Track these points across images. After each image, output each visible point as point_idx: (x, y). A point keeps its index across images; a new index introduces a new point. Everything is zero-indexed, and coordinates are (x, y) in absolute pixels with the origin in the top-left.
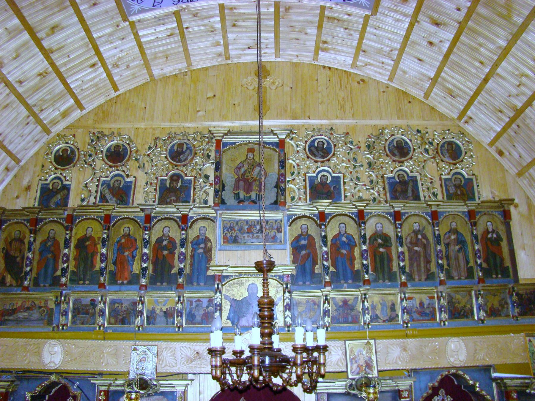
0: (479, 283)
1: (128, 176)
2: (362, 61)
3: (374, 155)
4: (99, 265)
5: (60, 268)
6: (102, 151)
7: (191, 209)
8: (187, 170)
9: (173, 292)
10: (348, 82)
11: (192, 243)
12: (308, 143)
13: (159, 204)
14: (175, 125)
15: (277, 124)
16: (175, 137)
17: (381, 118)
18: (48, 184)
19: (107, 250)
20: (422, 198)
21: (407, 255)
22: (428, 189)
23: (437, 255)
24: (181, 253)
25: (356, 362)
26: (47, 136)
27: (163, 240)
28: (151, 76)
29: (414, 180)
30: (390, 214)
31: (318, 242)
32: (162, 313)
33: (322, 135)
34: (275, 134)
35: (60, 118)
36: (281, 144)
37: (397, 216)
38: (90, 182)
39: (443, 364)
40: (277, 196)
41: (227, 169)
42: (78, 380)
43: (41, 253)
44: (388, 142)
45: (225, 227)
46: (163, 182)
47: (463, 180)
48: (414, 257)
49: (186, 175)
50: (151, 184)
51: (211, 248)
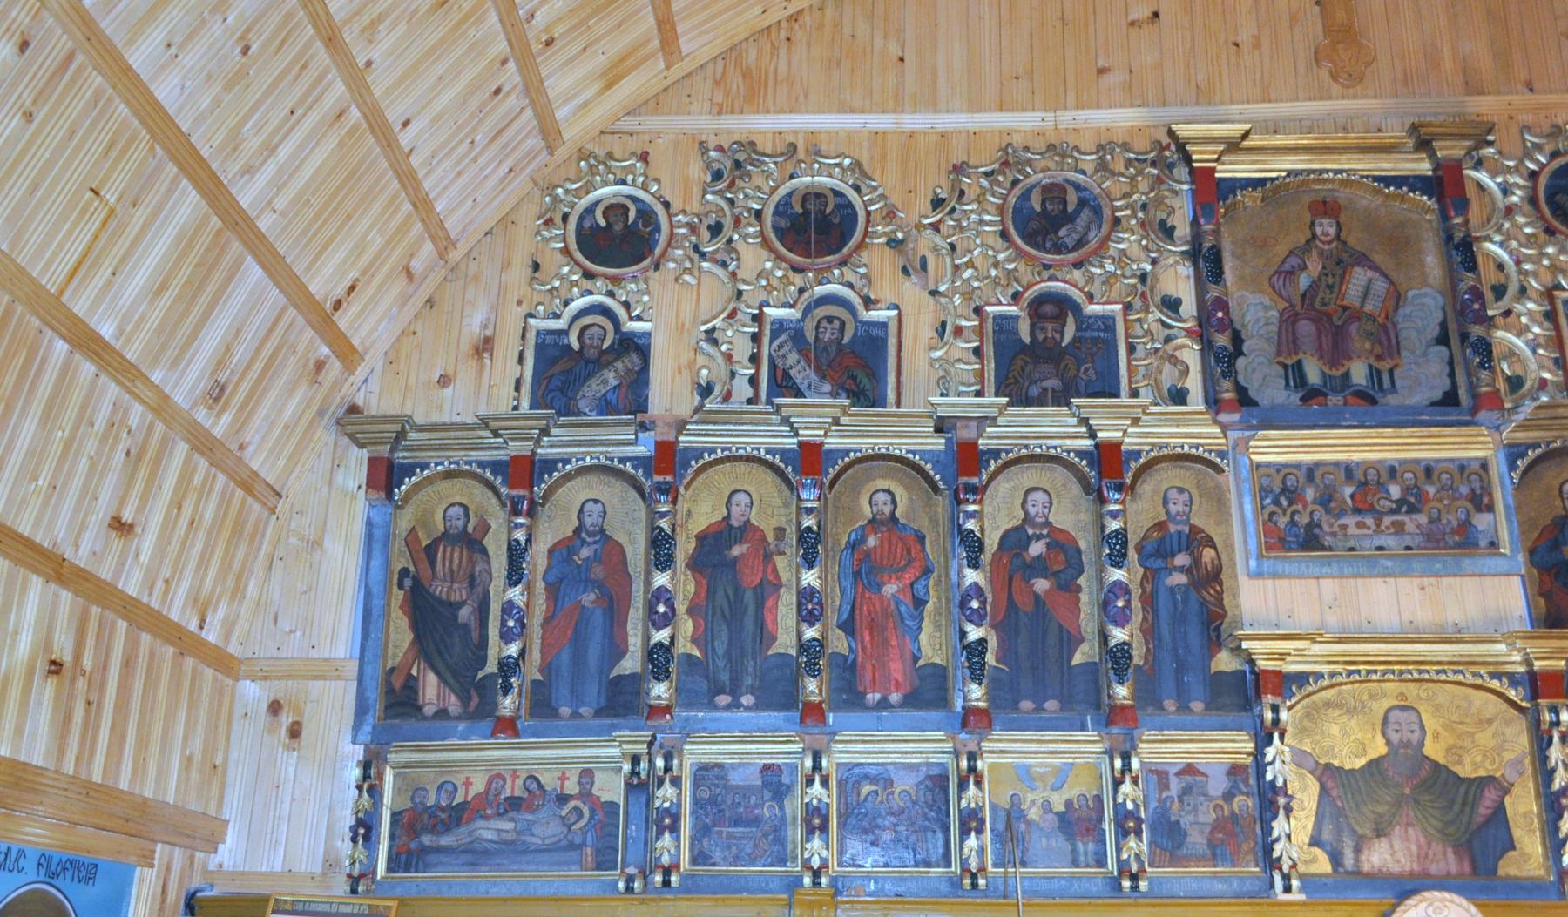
4: (787, 632)
9: (1091, 735)
12: (1543, 180)
14: (1025, 122)
18: (565, 332)
27: (1029, 539)
45: (1264, 492)
46: (1004, 325)
49: (1090, 298)
50: (958, 331)
51: (1218, 570)
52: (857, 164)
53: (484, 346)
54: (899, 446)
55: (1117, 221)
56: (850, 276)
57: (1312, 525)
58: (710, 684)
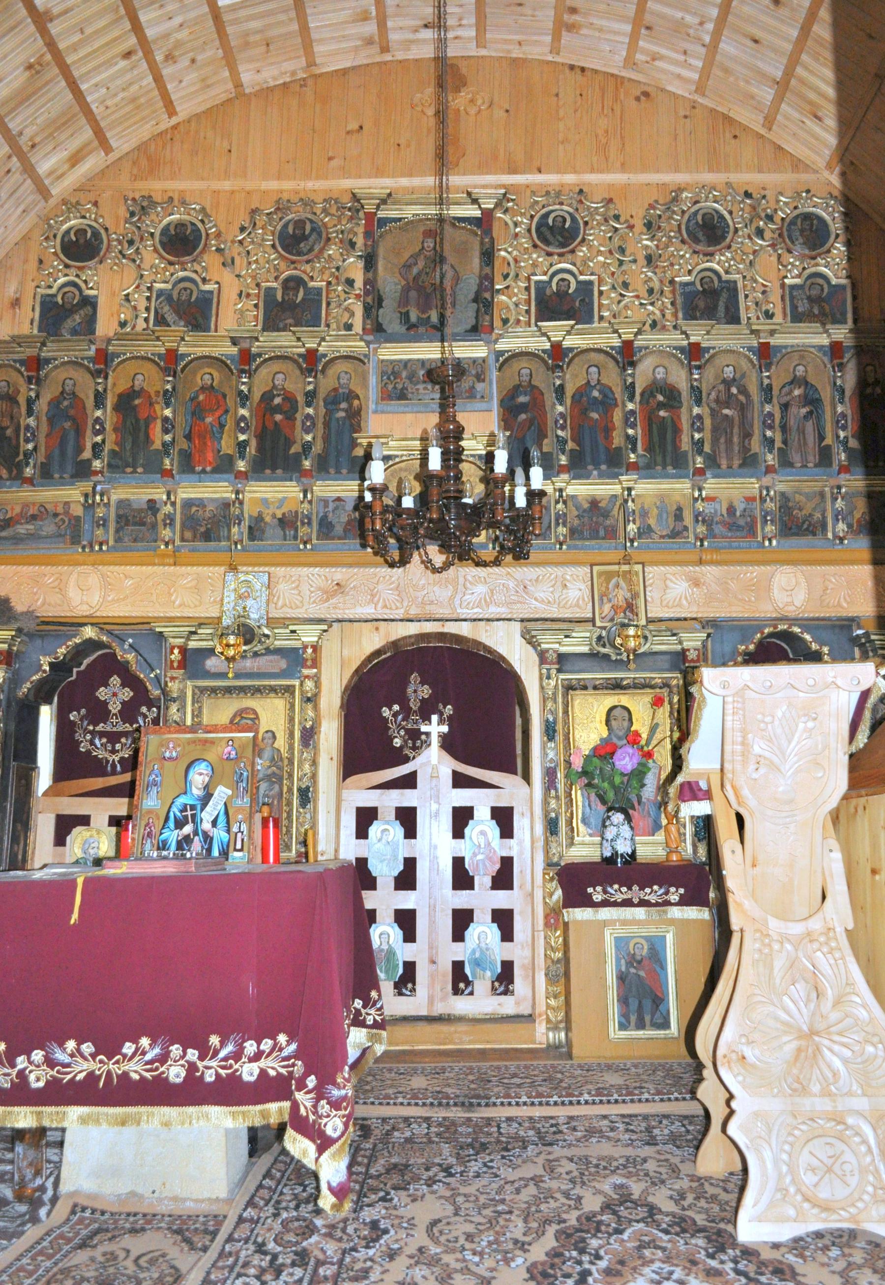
0: (839, 473)
1: (204, 280)
2: (645, 52)
3: (659, 240)
4: (159, 437)
5: (89, 446)
6: (152, 234)
7: (323, 339)
8: (313, 269)
9: (294, 483)
10: (616, 98)
11: (325, 401)
12: (536, 220)
13: (264, 330)
14: (288, 185)
15: (478, 185)
16: (289, 208)
17: (677, 170)
18: (55, 296)
19: (174, 412)
20: (744, 320)
21: (708, 422)
22: (757, 304)
23: (764, 422)
24: (308, 416)
25: (610, 601)
26: (42, 203)
27: (274, 396)
28: (238, 85)
29: (732, 289)
30: (682, 349)
31: (550, 397)
32: (276, 521)
33: (561, 204)
34: (475, 201)
35: (66, 166)
36: (484, 222)
37: (694, 352)
38: (135, 291)
39: (765, 610)
40: (477, 318)
41: (385, 269)
42: (131, 636)
43: (51, 421)
44: (686, 216)
45: (383, 373)
46: (270, 291)
47: (826, 286)
48: (721, 427)
49: (312, 278)
50: (248, 295)
52: (203, 210)
53: (16, 303)
54: (216, 352)
55: (329, 239)
56: (197, 267)
57: (404, 388)
58: (119, 464)
